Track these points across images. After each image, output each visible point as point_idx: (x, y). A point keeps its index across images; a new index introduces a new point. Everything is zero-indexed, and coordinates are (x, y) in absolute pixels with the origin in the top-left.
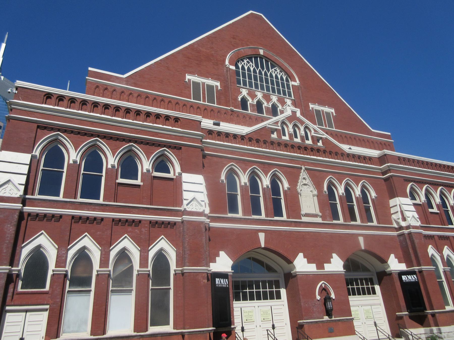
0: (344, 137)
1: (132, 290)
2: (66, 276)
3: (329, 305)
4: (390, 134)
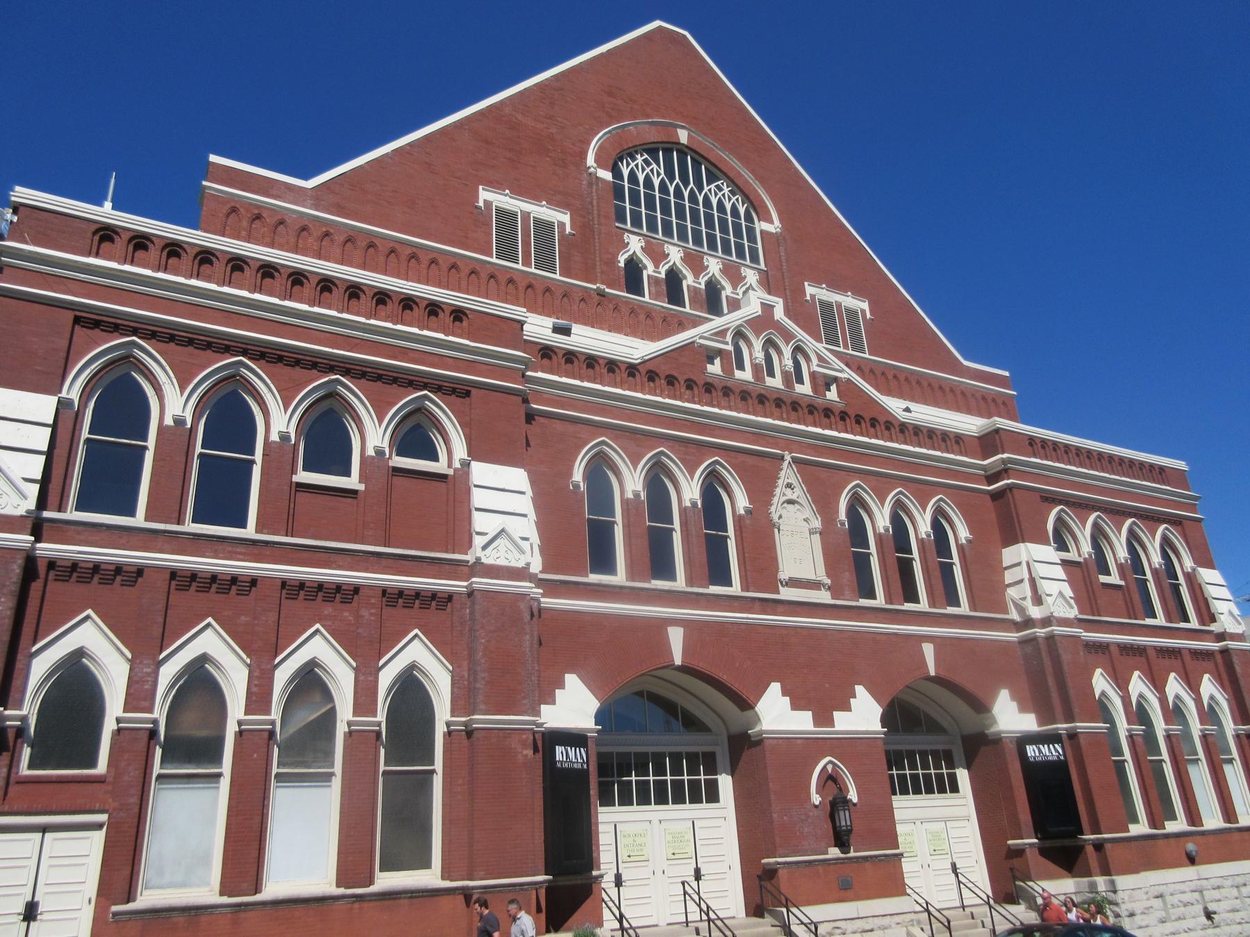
0: (890, 377)
1: (332, 774)
2: (153, 734)
3: (844, 819)
4: (1007, 374)
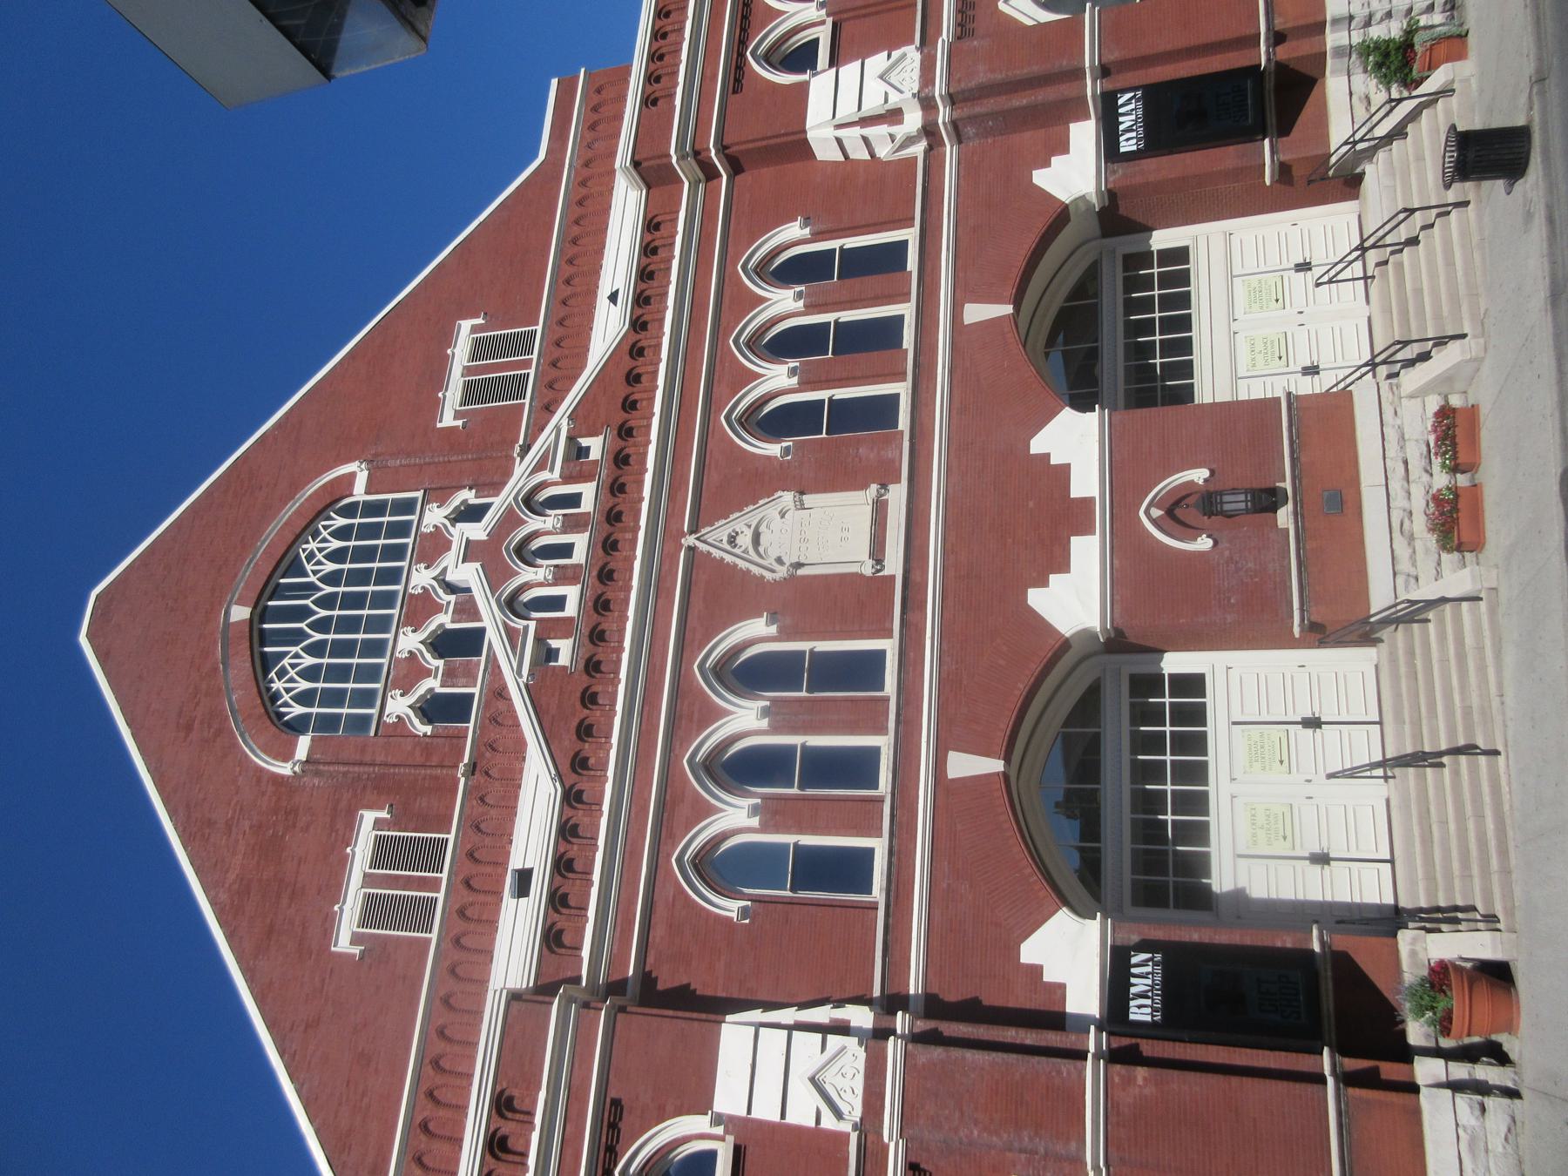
4: (554, 82)
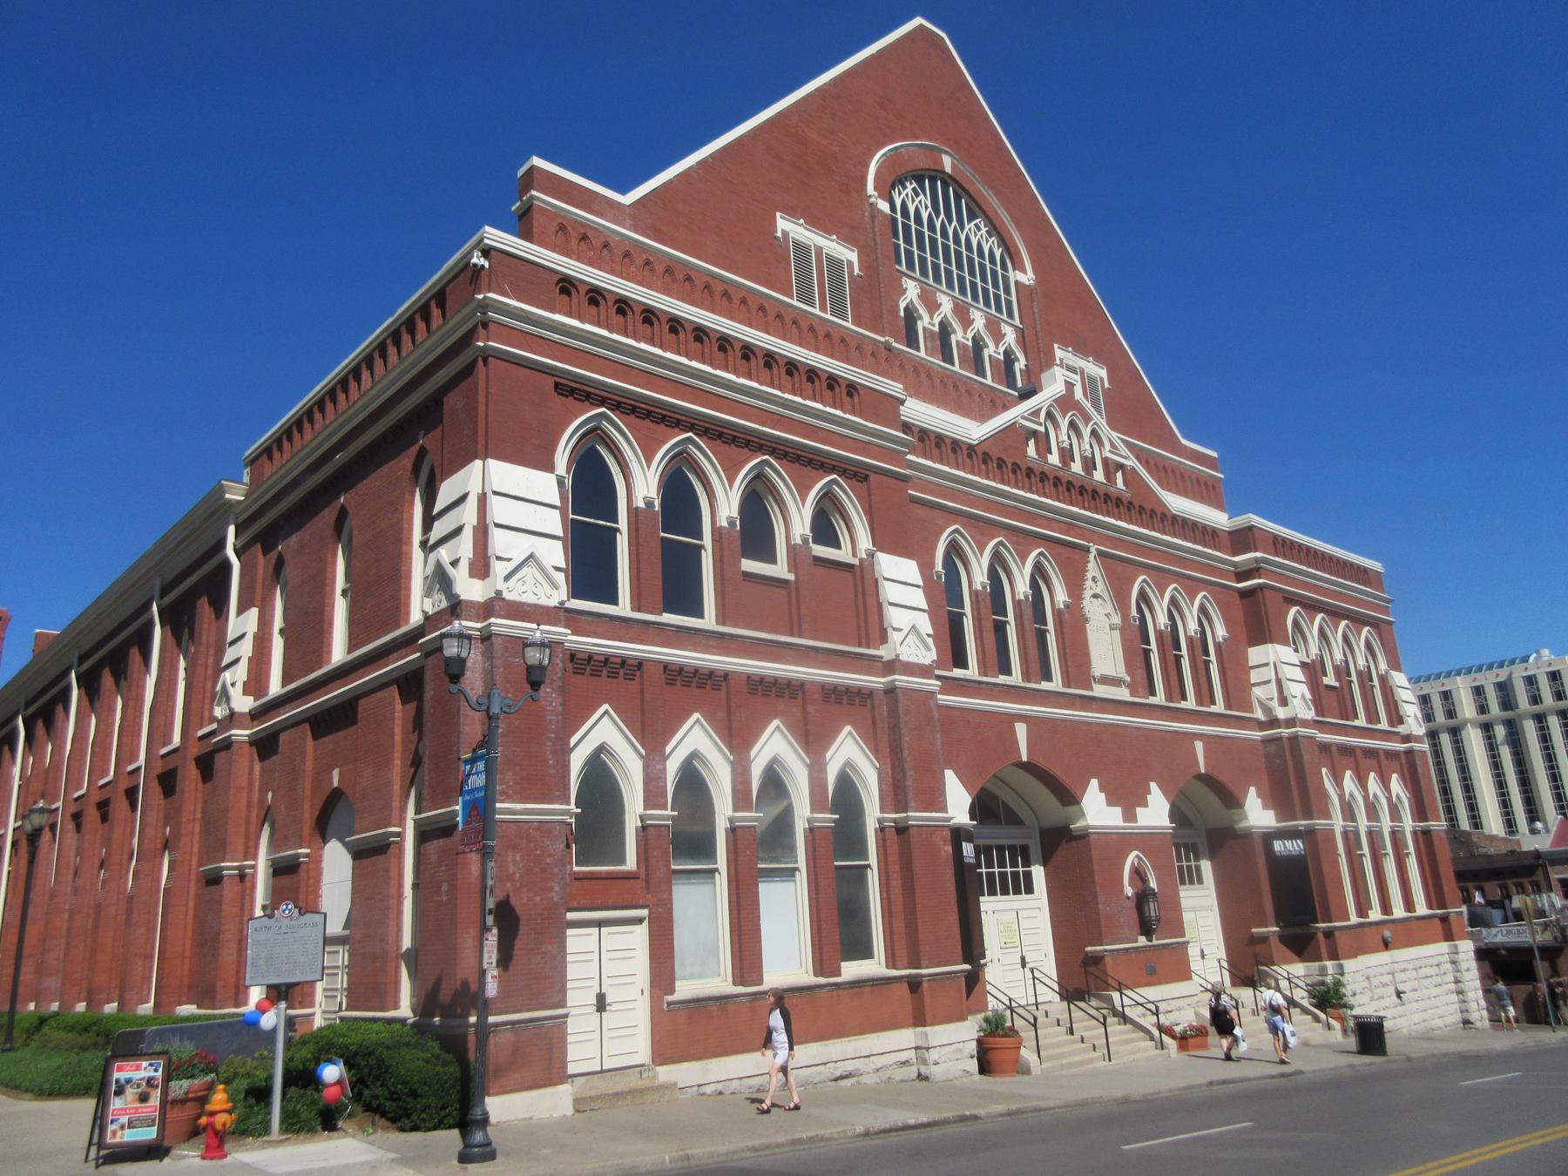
4: (1215, 454)
